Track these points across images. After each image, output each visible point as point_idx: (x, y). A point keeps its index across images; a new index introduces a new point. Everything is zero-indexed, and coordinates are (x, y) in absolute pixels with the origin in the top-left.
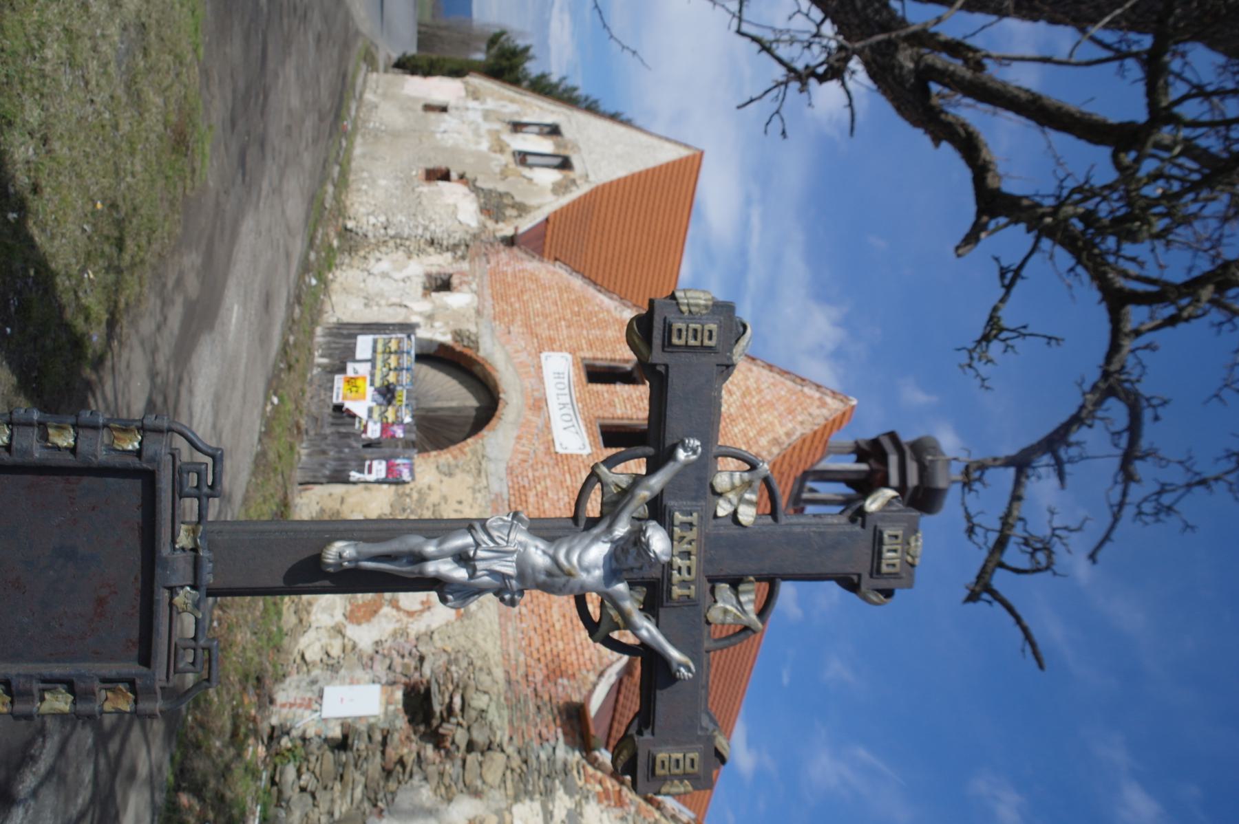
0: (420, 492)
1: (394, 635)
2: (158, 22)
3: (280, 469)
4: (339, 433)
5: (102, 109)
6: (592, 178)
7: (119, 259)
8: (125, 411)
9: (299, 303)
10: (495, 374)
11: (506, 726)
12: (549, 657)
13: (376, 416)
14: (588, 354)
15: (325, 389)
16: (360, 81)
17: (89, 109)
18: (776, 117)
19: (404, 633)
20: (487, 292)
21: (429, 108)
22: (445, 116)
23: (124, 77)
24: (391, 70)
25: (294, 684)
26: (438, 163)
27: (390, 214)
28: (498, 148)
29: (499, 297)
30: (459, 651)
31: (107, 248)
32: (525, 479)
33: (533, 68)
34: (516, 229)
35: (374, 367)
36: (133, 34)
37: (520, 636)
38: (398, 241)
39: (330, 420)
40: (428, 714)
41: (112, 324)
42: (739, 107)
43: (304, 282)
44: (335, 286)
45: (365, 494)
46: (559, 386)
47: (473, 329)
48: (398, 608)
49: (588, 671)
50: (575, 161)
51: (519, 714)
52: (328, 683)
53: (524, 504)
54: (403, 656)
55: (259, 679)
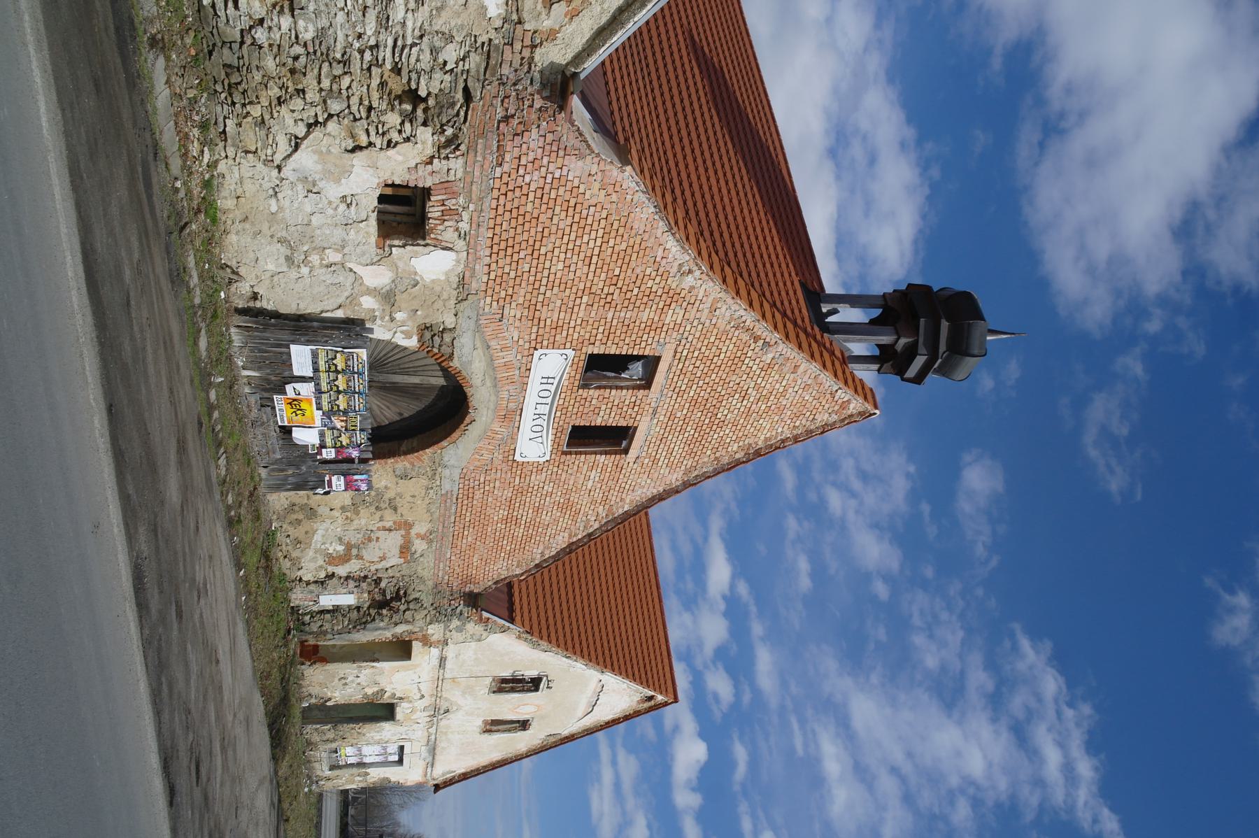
12: (465, 576)
46: (542, 394)
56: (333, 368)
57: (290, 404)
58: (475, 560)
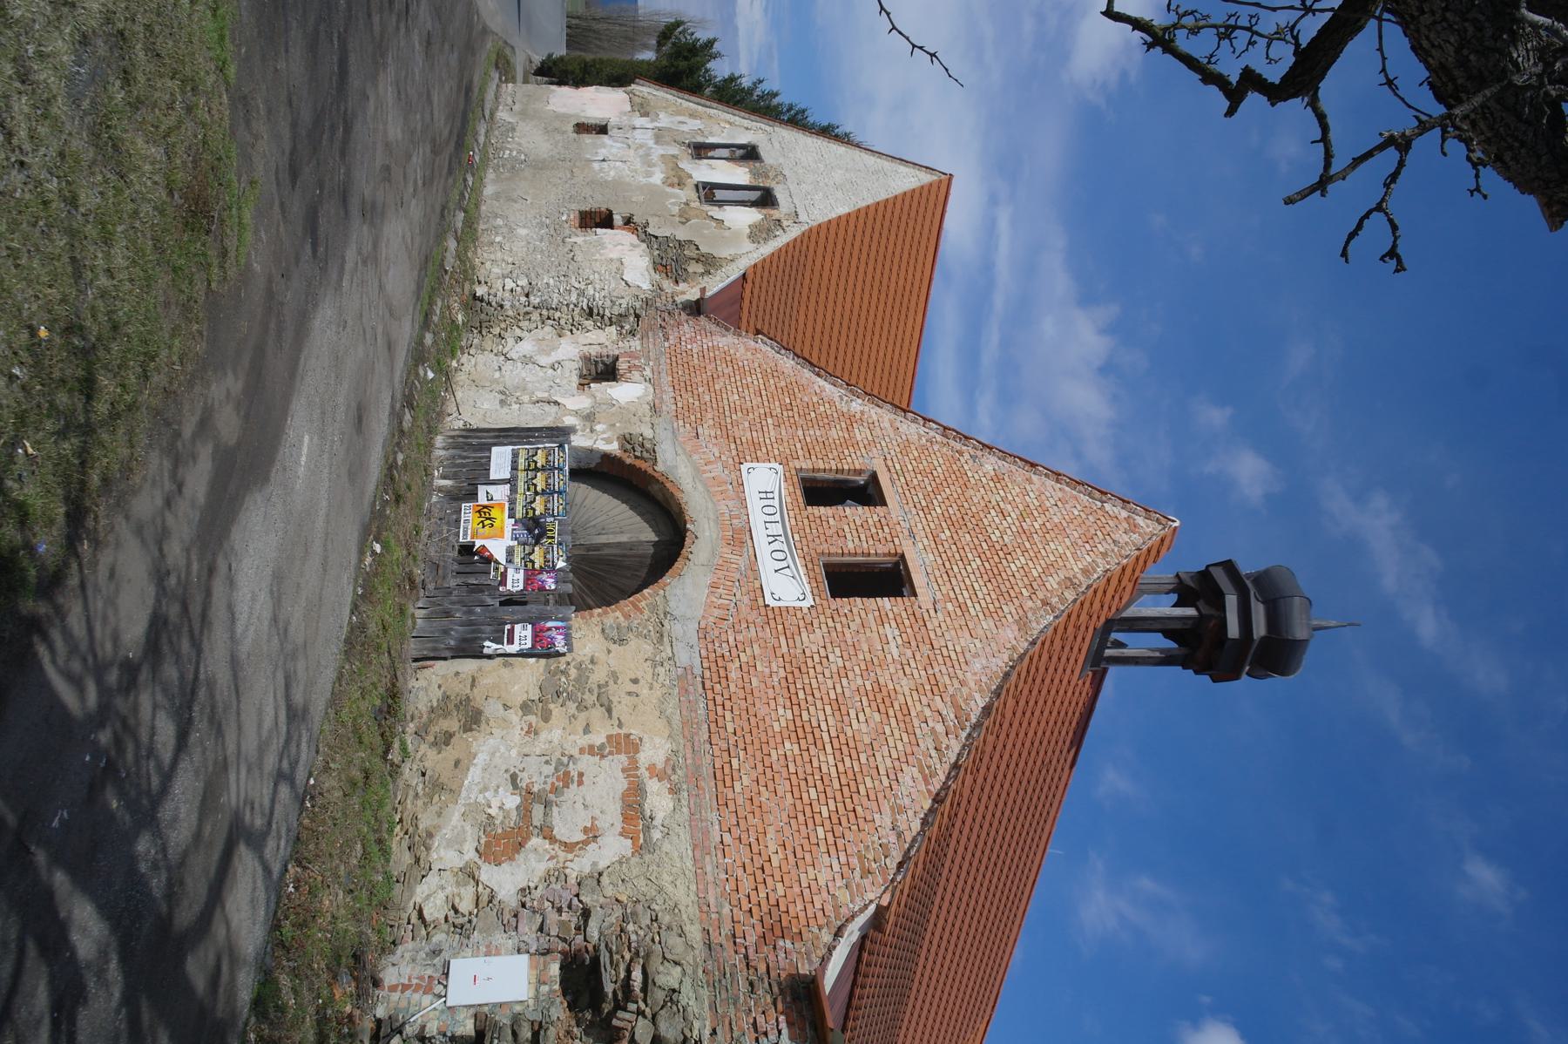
0: (579, 667)
1: (547, 879)
2: (148, 27)
3: (385, 646)
4: (468, 585)
5: (44, 175)
6: (803, 217)
7: (87, 411)
8: (109, 646)
9: (411, 407)
10: (678, 495)
11: (707, 1013)
13: (517, 560)
14: (806, 465)
15: (448, 523)
16: (490, 95)
17: (17, 177)
18: (1377, 217)
19: (559, 875)
20: (666, 379)
21: (582, 128)
22: (605, 138)
23: (88, 119)
24: (533, 78)
25: (407, 955)
26: (597, 202)
27: (533, 275)
28: (676, 180)
29: (683, 386)
30: (638, 901)
31: (62, 398)
32: (724, 645)
33: (719, 69)
34: (703, 290)
35: (514, 490)
36: (102, 48)
37: (724, 876)
38: (545, 312)
39: (456, 567)
40: (597, 994)
41: (77, 515)
42: (1289, 201)
43: (417, 374)
44: (461, 377)
45: (505, 672)
46: (767, 510)
47: (648, 433)
48: (552, 839)
49: (820, 928)
50: (780, 193)
51: (724, 995)
52: (455, 955)
53: (723, 681)
54: (560, 910)
55: (356, 957)
56: (532, 466)
57: (479, 511)
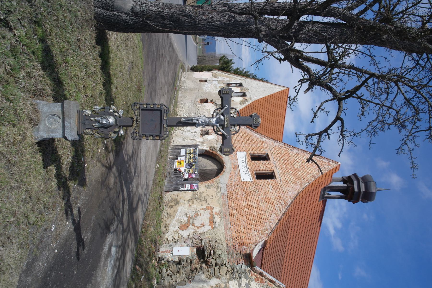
58: (242, 229)
